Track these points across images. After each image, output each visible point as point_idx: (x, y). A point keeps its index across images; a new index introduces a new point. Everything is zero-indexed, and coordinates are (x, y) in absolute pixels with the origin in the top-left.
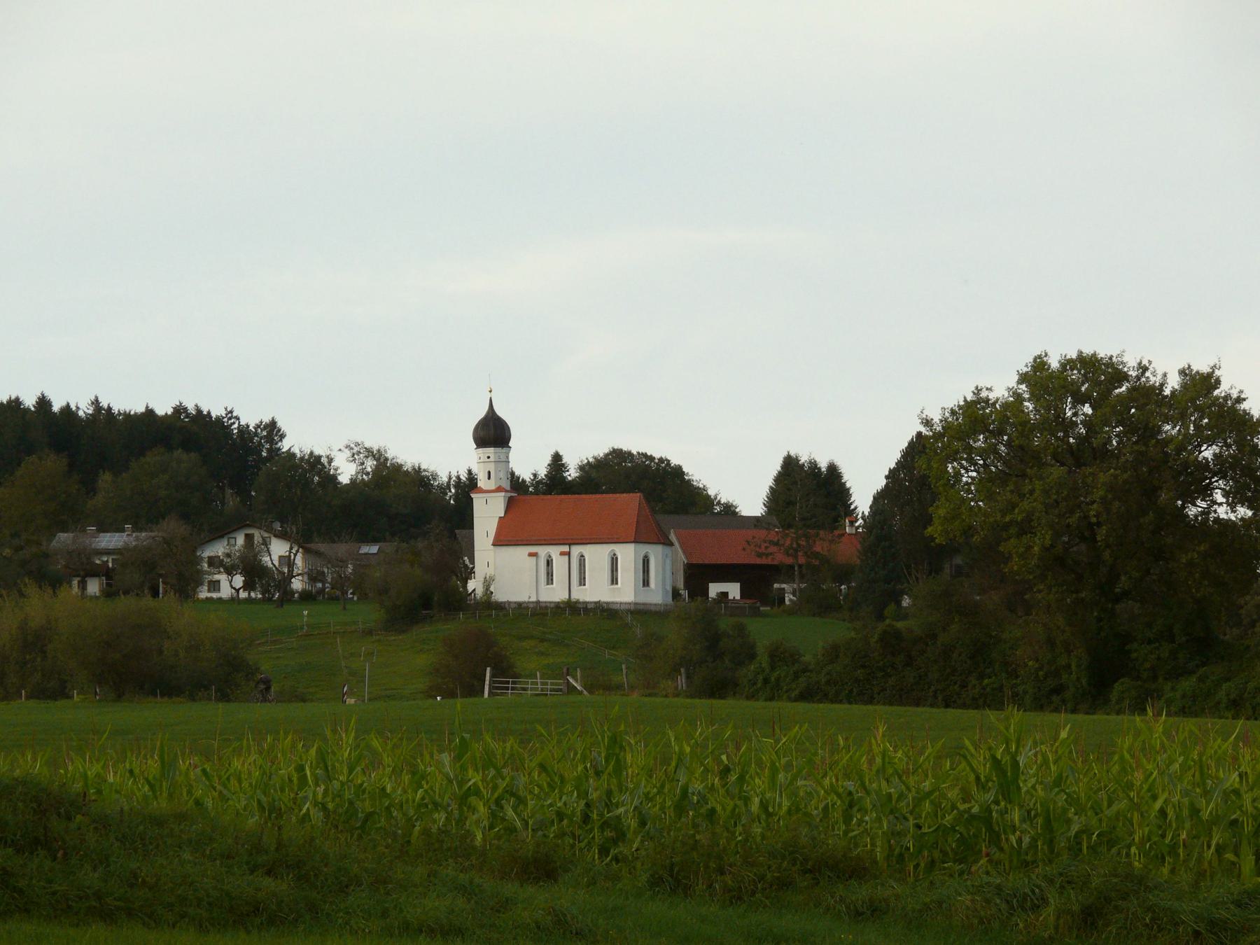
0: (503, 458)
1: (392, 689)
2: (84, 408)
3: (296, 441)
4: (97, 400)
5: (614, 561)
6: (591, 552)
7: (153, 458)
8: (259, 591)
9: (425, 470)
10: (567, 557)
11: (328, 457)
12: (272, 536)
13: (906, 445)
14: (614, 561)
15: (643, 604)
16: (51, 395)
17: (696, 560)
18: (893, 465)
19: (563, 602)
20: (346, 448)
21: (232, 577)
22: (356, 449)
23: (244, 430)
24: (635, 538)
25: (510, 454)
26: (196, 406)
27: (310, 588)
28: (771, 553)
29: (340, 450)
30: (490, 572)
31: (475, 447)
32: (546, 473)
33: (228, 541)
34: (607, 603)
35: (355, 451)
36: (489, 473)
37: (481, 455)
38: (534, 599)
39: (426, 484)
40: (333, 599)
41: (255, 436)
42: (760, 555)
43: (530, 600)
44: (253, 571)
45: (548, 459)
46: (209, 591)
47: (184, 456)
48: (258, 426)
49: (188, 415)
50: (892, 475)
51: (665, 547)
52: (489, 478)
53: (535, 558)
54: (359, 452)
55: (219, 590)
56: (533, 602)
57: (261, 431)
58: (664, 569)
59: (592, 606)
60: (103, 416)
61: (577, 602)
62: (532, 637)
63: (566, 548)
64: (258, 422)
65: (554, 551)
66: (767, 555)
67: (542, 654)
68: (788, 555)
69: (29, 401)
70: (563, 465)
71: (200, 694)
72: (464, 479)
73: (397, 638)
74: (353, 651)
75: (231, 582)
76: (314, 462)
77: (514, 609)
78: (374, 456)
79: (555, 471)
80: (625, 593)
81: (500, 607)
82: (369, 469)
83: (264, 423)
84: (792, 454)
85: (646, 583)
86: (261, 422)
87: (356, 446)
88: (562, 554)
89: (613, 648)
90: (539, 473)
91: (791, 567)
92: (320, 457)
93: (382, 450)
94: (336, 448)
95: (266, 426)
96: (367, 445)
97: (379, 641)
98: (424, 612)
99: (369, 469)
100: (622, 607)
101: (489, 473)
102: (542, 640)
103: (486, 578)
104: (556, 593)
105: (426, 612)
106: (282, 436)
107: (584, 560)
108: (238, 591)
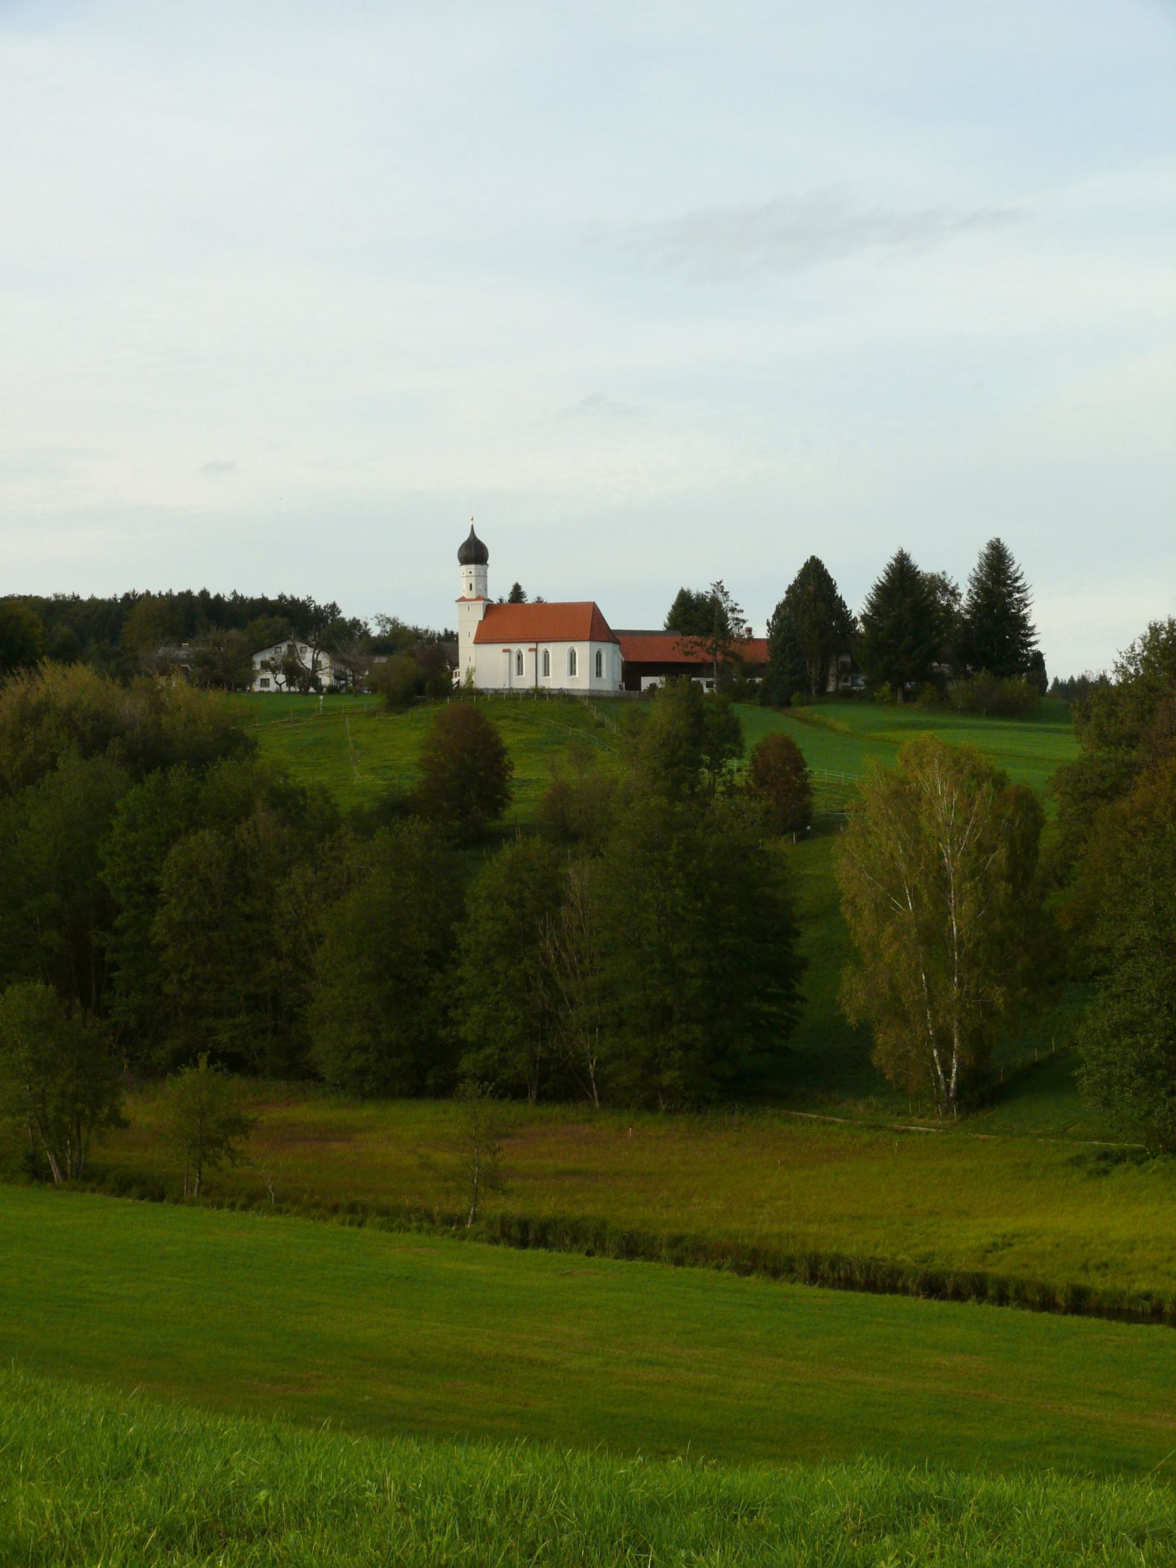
3: (347, 614)
4: (235, 592)
5: (573, 656)
6: (552, 648)
7: (260, 621)
10: (534, 653)
13: (802, 566)
14: (573, 656)
15: (598, 691)
16: (209, 589)
18: (792, 583)
19: (532, 689)
22: (381, 618)
23: (317, 609)
30: (472, 664)
34: (568, 690)
36: (471, 585)
40: (349, 692)
42: (687, 654)
44: (293, 671)
45: (510, 589)
46: (261, 686)
48: (326, 607)
49: (286, 600)
50: (791, 590)
51: (615, 645)
52: (471, 589)
54: (383, 620)
55: (269, 686)
61: (543, 689)
63: (533, 646)
65: (524, 648)
66: (692, 654)
67: (515, 731)
69: (196, 592)
71: (172, 769)
75: (275, 679)
76: (355, 623)
77: (491, 695)
80: (582, 682)
81: (480, 693)
82: (388, 630)
85: (599, 674)
88: (530, 650)
89: (574, 726)
91: (712, 664)
95: (331, 606)
99: (388, 630)
100: (578, 694)
101: (471, 585)
102: (516, 720)
104: (525, 682)
108: (280, 685)
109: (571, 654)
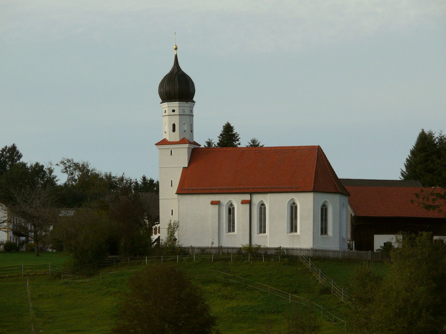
0: (187, 112)
5: (293, 209)
9: (114, 177)
10: (248, 206)
14: (293, 209)
17: (362, 214)
19: (245, 248)
20: (61, 163)
22: (68, 164)
24: (314, 188)
25: (194, 108)
27: (15, 241)
29: (57, 165)
30: (175, 218)
31: (161, 101)
32: (219, 142)
34: (287, 249)
35: (67, 165)
36: (174, 125)
37: (167, 109)
38: (216, 245)
39: (114, 186)
40: (31, 250)
41: (2, 157)
42: (428, 207)
43: (213, 246)
45: (220, 130)
52: (174, 130)
56: (215, 248)
57: (6, 153)
59: (273, 252)
61: (259, 248)
62: (215, 281)
63: (247, 197)
64: (4, 147)
66: (434, 207)
70: (234, 135)
72: (141, 183)
73: (84, 281)
78: (80, 169)
81: (184, 252)
83: (8, 148)
84: (427, 131)
85: (324, 231)
86: (6, 147)
87: (68, 162)
88: (244, 202)
89: (295, 292)
90: (212, 142)
92: (43, 166)
93: (85, 165)
94: (54, 163)
95: (10, 149)
96: (75, 161)
97: (67, 283)
98: (110, 257)
101: (174, 125)
102: (227, 284)
103: (170, 224)
105: (113, 256)
107: (265, 208)
109: (292, 207)
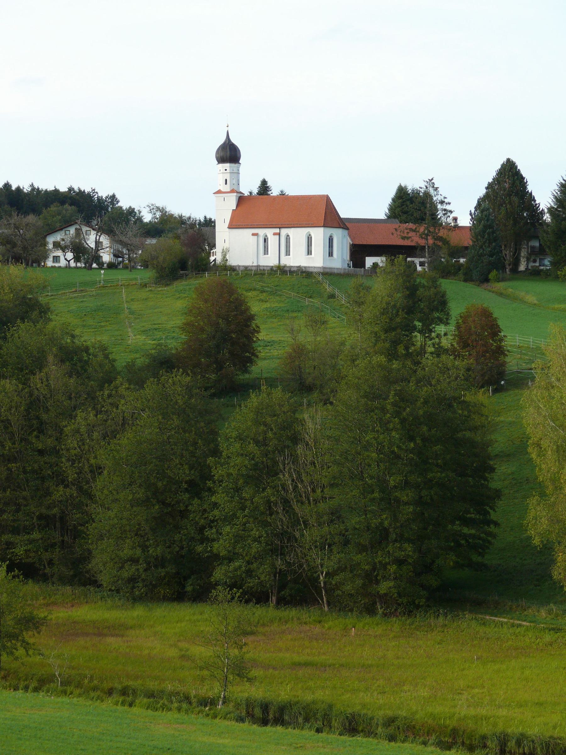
0: (235, 171)
1: (158, 324)
2: (27, 189)
3: (124, 204)
4: (32, 184)
5: (309, 239)
6: (292, 232)
7: (53, 208)
8: (83, 262)
9: (184, 216)
10: (278, 236)
11: (139, 211)
12: (91, 229)
16: (11, 182)
17: (357, 242)
21: (65, 253)
22: (152, 207)
23: (100, 199)
26: (79, 188)
27: (114, 261)
28: (410, 237)
30: (226, 245)
31: (217, 163)
33: (65, 232)
34: (305, 267)
35: (151, 208)
36: (226, 180)
38: (255, 264)
39: (184, 223)
45: (259, 184)
46: (53, 262)
47: (69, 208)
48: (107, 197)
50: (490, 186)
52: (226, 184)
53: (256, 237)
54: (154, 209)
56: (255, 266)
58: (342, 243)
59: (295, 269)
60: (36, 192)
61: (285, 266)
62: (255, 289)
63: (277, 230)
65: (269, 232)
68: (422, 238)
70: (268, 187)
74: (133, 297)
76: (131, 211)
78: (160, 210)
79: (263, 190)
81: (233, 269)
82: (158, 217)
84: (403, 185)
85: (331, 254)
88: (275, 234)
89: (311, 297)
91: (423, 248)
93: (164, 208)
94: (142, 207)
95: (111, 197)
97: (151, 291)
98: (181, 272)
99: (158, 217)
101: (226, 180)
102: (263, 292)
104: (270, 260)
106: (118, 202)
107: (289, 238)
108: (69, 261)
109: (308, 238)
